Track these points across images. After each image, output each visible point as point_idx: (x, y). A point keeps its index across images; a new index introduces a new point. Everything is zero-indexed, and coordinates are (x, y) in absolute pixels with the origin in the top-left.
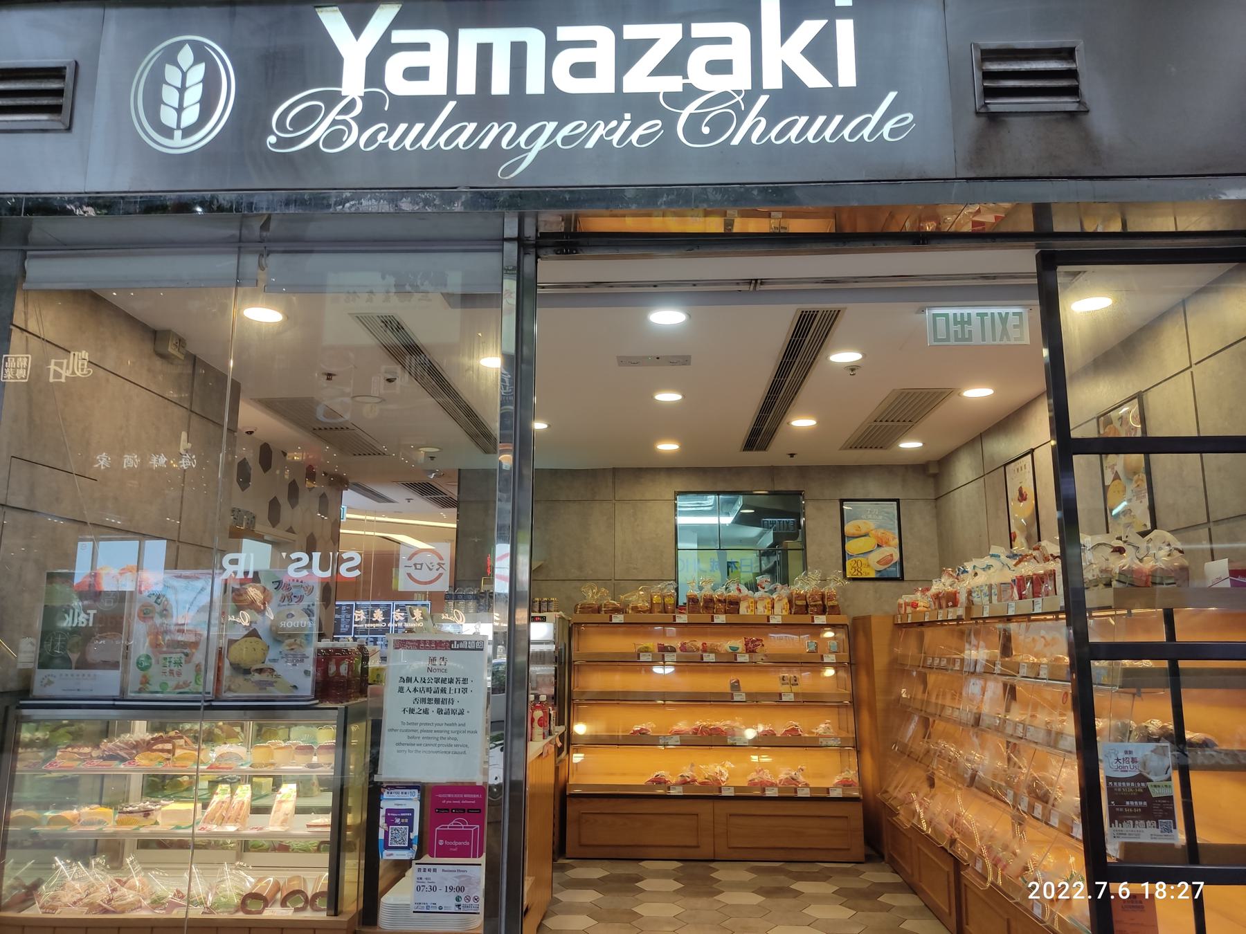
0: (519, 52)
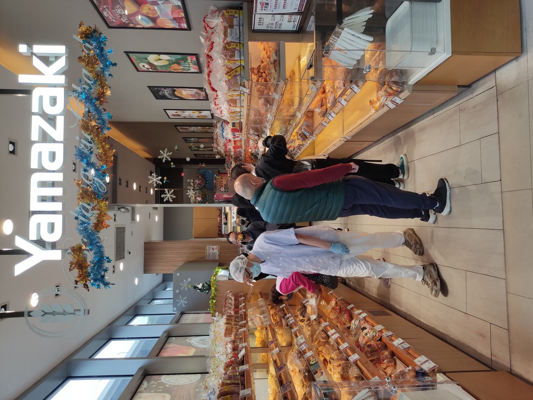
0: (43, 184)
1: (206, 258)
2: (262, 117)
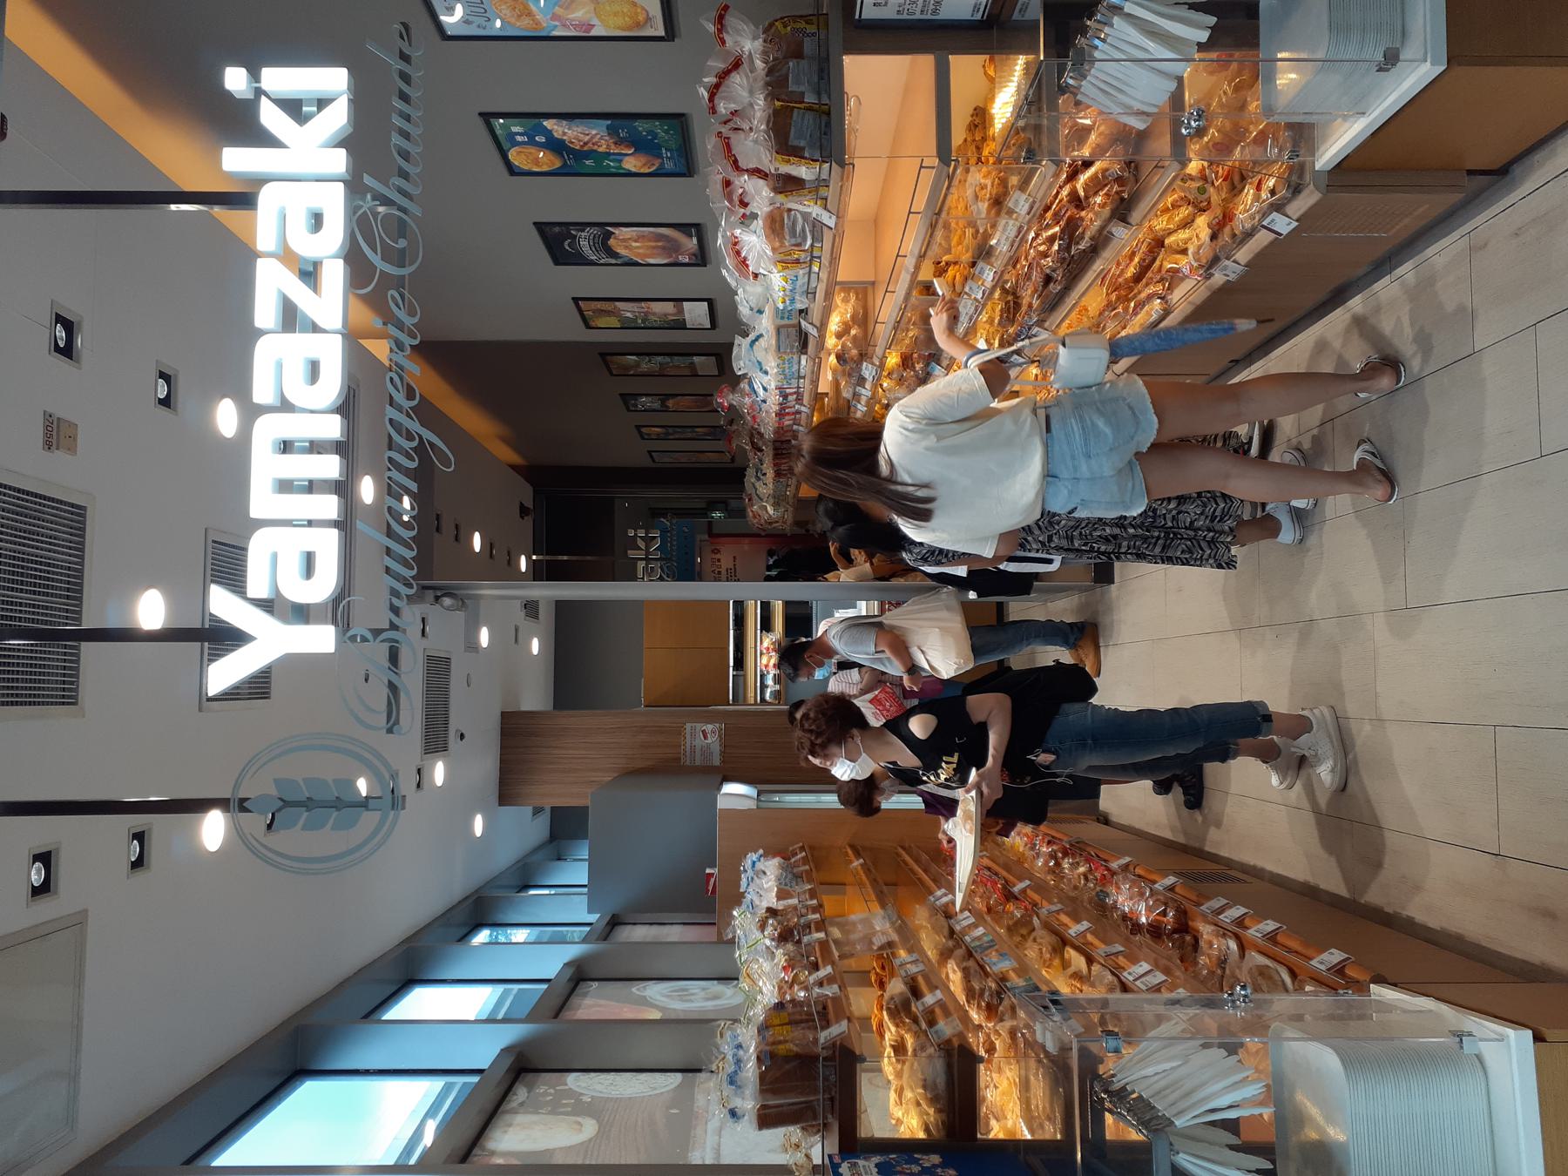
1: (682, 761)
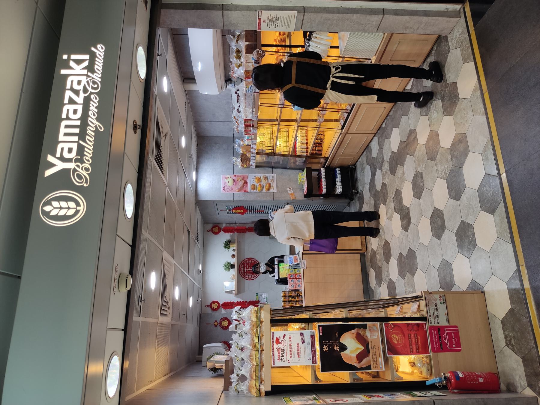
0: (67, 126)
2: (250, 358)
